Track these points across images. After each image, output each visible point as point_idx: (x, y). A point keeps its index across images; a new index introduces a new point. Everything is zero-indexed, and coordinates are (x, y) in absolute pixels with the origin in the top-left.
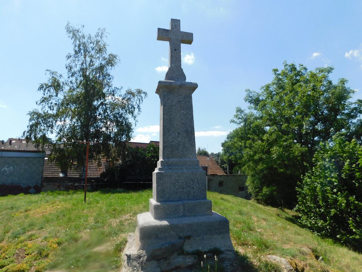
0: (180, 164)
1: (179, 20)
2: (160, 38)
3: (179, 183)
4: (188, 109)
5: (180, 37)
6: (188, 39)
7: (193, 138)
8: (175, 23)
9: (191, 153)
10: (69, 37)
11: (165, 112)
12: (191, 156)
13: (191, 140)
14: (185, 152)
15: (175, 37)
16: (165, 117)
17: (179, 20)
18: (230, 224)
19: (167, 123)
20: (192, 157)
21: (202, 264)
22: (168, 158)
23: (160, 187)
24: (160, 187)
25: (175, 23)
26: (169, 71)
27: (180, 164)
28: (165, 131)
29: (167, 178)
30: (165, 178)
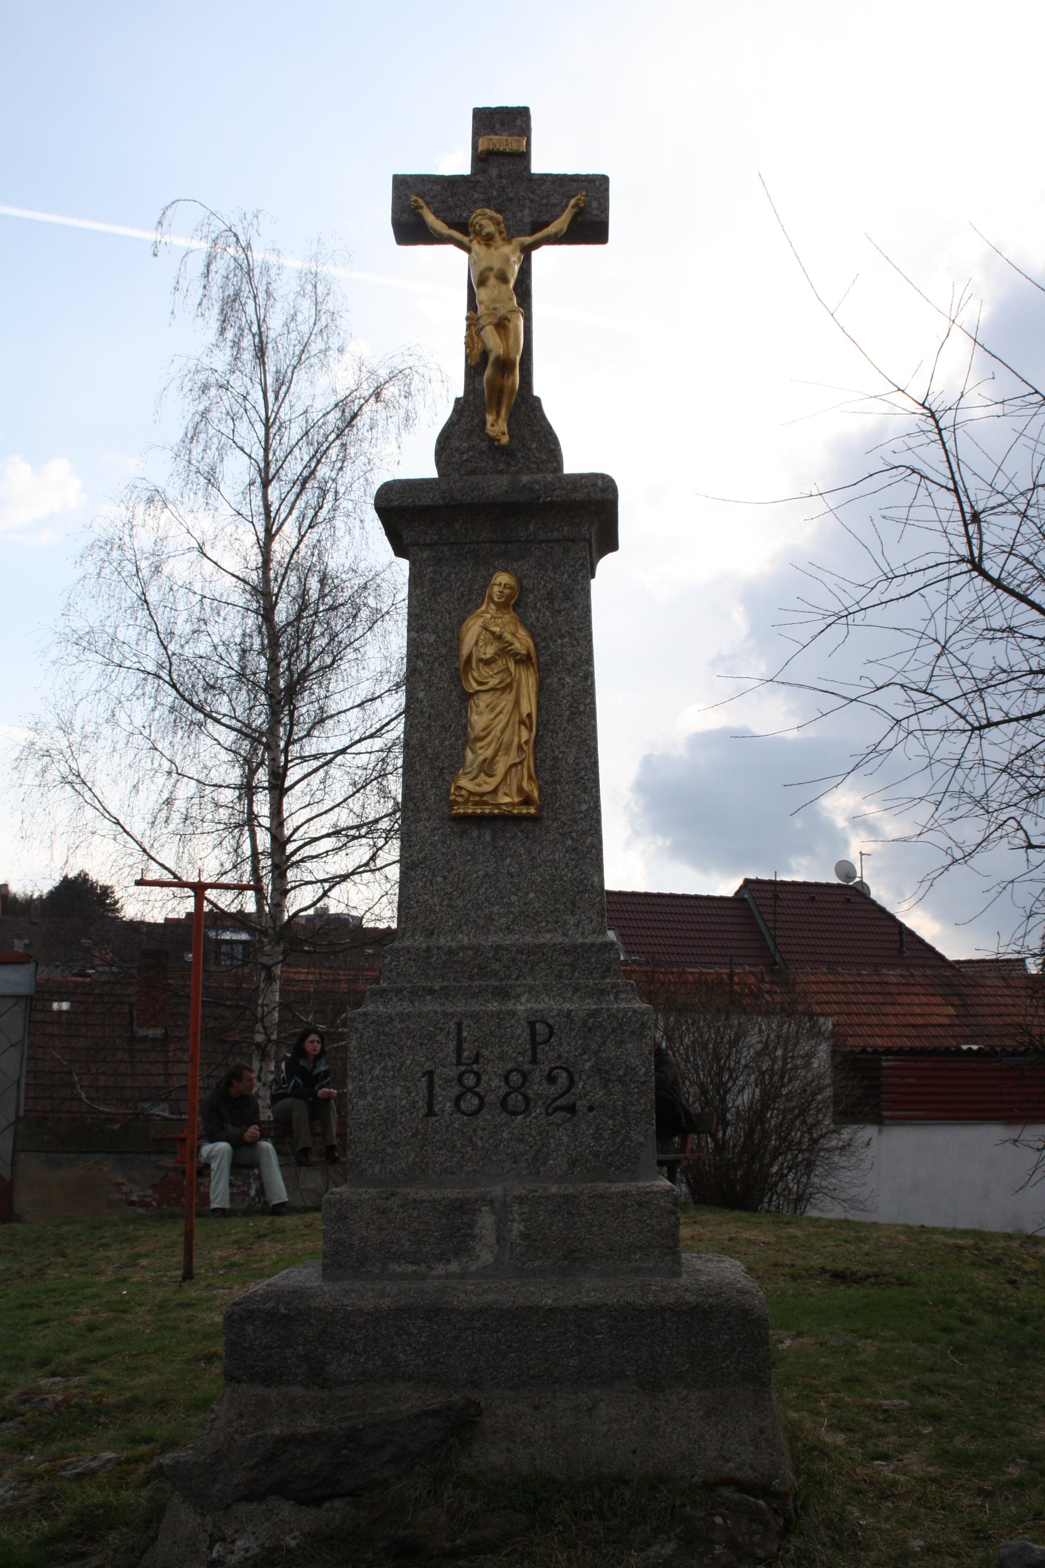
0: (497, 966)
1: (526, 110)
2: (410, 229)
3: (485, 1078)
4: (562, 637)
5: (526, 212)
6: (582, 211)
7: (584, 807)
8: (502, 130)
9: (573, 903)
10: (36, 728)
11: (420, 663)
12: (572, 920)
13: (575, 821)
14: (532, 895)
15: (504, 202)
16: (421, 695)
17: (526, 110)
18: (880, 894)
19: (429, 726)
20: (577, 925)
21: (619, 1187)
22: (432, 933)
23: (369, 1098)
24: (369, 1098)
25: (502, 130)
26: (459, 420)
27: (497, 966)
28: (417, 773)
29: (411, 1048)
30: (401, 1049)
